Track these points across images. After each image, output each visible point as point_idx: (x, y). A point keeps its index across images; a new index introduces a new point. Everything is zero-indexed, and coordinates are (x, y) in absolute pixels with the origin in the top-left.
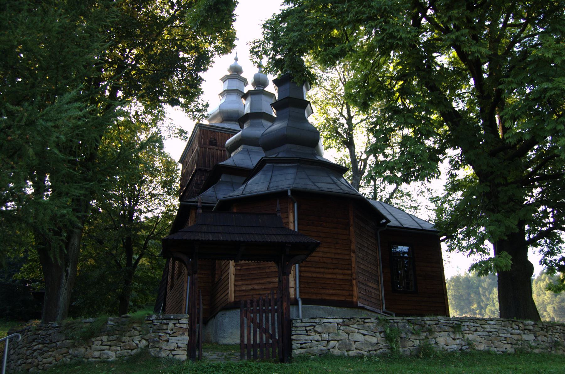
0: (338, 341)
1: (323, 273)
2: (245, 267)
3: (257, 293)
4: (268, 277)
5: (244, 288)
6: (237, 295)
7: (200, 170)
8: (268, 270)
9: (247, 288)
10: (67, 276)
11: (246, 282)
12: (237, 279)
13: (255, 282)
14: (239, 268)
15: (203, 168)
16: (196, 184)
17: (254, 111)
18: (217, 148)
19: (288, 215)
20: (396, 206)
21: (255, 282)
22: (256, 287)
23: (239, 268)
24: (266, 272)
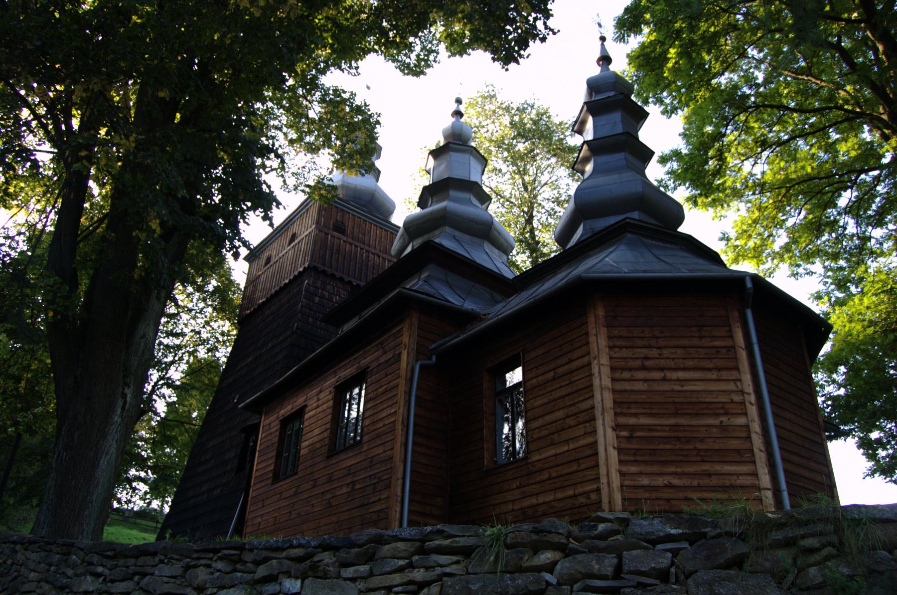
2: (639, 434)
3: (681, 495)
4: (703, 461)
5: (645, 481)
6: (627, 495)
8: (700, 446)
9: (654, 483)
10: (123, 408)
11: (649, 469)
12: (623, 458)
13: (672, 469)
14: (624, 433)
17: (600, 135)
18: (345, 239)
19: (730, 331)
20: (269, 426)
21: (672, 469)
22: (676, 482)
23: (624, 433)
24: (696, 449)
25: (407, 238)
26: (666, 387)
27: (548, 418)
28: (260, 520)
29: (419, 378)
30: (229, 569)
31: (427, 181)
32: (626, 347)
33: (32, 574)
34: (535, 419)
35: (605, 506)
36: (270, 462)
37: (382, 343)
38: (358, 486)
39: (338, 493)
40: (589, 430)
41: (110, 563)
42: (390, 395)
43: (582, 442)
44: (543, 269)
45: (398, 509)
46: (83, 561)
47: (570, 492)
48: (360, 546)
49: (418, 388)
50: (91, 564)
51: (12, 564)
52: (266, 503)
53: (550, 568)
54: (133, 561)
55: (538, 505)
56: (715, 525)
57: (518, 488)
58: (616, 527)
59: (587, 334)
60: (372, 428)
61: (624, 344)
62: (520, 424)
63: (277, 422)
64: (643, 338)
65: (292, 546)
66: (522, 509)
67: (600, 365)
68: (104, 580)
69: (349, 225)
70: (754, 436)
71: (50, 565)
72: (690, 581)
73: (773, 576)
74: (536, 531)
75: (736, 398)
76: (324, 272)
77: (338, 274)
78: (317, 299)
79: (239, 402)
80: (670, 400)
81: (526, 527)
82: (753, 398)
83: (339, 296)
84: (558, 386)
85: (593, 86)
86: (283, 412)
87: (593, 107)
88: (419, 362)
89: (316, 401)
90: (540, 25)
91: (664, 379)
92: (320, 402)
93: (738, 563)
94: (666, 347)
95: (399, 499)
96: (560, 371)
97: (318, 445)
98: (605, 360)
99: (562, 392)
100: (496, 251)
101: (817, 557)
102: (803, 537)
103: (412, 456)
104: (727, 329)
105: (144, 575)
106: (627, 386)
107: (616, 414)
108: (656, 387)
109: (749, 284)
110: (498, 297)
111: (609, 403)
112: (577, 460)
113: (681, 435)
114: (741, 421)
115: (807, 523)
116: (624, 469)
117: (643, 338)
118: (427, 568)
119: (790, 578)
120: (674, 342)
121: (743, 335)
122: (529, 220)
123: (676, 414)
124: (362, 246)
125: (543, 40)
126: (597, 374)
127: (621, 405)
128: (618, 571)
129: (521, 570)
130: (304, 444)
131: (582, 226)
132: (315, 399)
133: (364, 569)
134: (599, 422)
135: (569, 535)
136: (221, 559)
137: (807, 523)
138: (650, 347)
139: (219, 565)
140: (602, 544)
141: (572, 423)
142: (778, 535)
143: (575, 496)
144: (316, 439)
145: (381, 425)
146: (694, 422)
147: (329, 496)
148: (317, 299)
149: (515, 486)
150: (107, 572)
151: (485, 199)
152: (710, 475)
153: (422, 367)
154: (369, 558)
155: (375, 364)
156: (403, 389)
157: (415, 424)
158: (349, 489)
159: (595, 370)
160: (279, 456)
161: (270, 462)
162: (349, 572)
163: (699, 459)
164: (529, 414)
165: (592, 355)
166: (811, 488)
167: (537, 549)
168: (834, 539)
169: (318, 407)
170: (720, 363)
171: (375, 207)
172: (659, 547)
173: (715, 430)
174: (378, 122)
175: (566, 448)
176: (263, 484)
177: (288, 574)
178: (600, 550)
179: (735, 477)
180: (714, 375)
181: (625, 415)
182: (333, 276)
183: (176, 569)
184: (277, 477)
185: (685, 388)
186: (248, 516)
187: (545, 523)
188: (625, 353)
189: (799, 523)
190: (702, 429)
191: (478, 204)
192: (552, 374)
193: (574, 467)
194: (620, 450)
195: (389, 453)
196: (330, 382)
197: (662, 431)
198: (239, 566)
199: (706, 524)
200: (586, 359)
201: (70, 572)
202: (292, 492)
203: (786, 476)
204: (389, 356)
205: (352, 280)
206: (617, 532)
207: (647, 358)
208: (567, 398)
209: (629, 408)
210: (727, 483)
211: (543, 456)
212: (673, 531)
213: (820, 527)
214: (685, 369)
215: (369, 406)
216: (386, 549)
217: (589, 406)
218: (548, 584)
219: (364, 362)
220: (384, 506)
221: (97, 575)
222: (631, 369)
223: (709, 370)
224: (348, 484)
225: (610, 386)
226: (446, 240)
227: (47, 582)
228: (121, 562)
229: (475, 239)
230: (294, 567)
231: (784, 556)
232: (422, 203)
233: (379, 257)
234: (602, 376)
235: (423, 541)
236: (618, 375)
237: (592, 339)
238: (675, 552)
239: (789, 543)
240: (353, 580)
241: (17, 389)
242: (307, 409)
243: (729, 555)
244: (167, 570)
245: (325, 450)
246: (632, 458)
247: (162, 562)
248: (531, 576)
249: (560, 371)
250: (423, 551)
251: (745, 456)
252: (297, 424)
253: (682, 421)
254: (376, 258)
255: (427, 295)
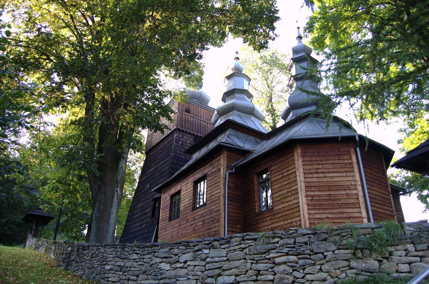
0: (339, 269)
1: (379, 208)
4: (340, 208)
5: (318, 216)
7: (179, 129)
8: (339, 202)
10: (117, 196)
12: (309, 208)
13: (328, 211)
14: (310, 198)
15: (181, 129)
16: (176, 139)
18: (190, 115)
19: (351, 156)
20: (165, 198)
22: (330, 216)
23: (310, 198)
24: (337, 203)
25: (218, 116)
26: (325, 180)
27: (281, 193)
28: (165, 237)
29: (228, 178)
30: (185, 248)
31: (225, 90)
32: (310, 165)
33: (110, 256)
34: (275, 193)
35: (303, 226)
36: (167, 213)
37: (212, 164)
38: (206, 222)
39: (198, 225)
40: (296, 197)
41: (142, 250)
42: (217, 185)
43: (293, 202)
44: (276, 131)
45: (223, 230)
46: (131, 250)
47: (290, 221)
48: (225, 239)
49: (228, 182)
50: (135, 250)
51: (98, 253)
52: (167, 230)
53: (277, 243)
54: (151, 248)
55: (278, 226)
56: (320, 230)
57: (270, 220)
58: (294, 231)
59: (294, 160)
60: (210, 198)
61: (308, 163)
62: (270, 192)
63: (169, 196)
64: (316, 161)
65: (205, 241)
66: (271, 228)
67: (299, 172)
68: (141, 255)
69: (192, 109)
70: (360, 198)
71: (117, 252)
72: (312, 244)
73: (334, 243)
74: (273, 233)
75: (353, 183)
76: (182, 131)
77: (188, 131)
78: (180, 143)
79: (150, 188)
80: (327, 185)
81: (271, 232)
82: (359, 183)
83: (189, 141)
84: (283, 180)
85: (295, 51)
86: (171, 192)
87: (296, 60)
88: (228, 172)
89: (185, 187)
90: (271, 33)
91: (325, 177)
92: (187, 188)
93: (325, 240)
94: (325, 164)
95: (223, 226)
96: (284, 174)
97: (188, 206)
98: (301, 170)
99: (286, 183)
100: (257, 119)
101: (346, 238)
102: (342, 233)
103: (228, 209)
104: (349, 156)
105: (155, 252)
106: (310, 180)
107: (306, 191)
108: (321, 180)
109: (357, 138)
110: (258, 140)
111: (303, 187)
112: (292, 209)
113: (331, 198)
114: (355, 192)
115: (344, 229)
116: (310, 212)
117: (316, 161)
118: (245, 244)
119: (338, 244)
120: (329, 162)
121: (355, 158)
122: (270, 101)
123: (329, 190)
124: (198, 118)
125: (274, 39)
126: (298, 176)
127: (308, 187)
128: (295, 243)
129: (270, 243)
130: (181, 206)
131: (292, 113)
132: (185, 187)
133: (227, 245)
134: (300, 194)
135: (282, 234)
136: (182, 246)
137: (344, 229)
138: (319, 164)
139: (182, 247)
140: (291, 236)
141: (290, 195)
142: (336, 232)
143: (291, 223)
144: (187, 203)
145: (214, 197)
146: (336, 193)
147: (194, 226)
148: (180, 143)
149: (268, 219)
150: (141, 252)
151: (250, 96)
152: (343, 213)
153: (229, 173)
154: (229, 242)
155: (210, 172)
156: (222, 182)
157: (228, 197)
158: (202, 223)
159: (298, 174)
160: (171, 210)
161: (167, 213)
162: (223, 247)
163: (338, 207)
164: (273, 188)
165: (296, 168)
166: (385, 216)
167: (274, 238)
168: (350, 233)
169: (187, 190)
170: (346, 169)
171: (202, 100)
172: (305, 236)
173: (344, 196)
174: (204, 66)
175: (287, 204)
176: (165, 222)
177: (205, 248)
178: (290, 238)
179: (353, 214)
180: (344, 174)
181: (310, 191)
182: (186, 132)
183: (167, 249)
184: (170, 219)
185: (333, 180)
186: (159, 235)
187: (276, 231)
188: (309, 167)
189: (341, 229)
190: (340, 195)
191: (248, 100)
192: (281, 176)
193: (291, 212)
194: (308, 205)
195: (218, 208)
196: (190, 180)
197: (324, 197)
198: (188, 247)
199: (318, 230)
200: (294, 170)
201: (126, 253)
202: (178, 225)
203: (372, 212)
204: (216, 169)
205: (194, 133)
206: (295, 233)
207: (318, 169)
208: (287, 185)
209: (311, 188)
210: (349, 216)
211: (279, 208)
212: (309, 232)
213: (346, 230)
214: (332, 172)
215: (209, 189)
216: (233, 240)
217: (296, 188)
218: (277, 246)
219: (205, 172)
220: (217, 229)
221: (138, 254)
222: (311, 173)
223: (342, 172)
224: (202, 221)
225: (303, 180)
226: (234, 117)
227: (117, 257)
228: (146, 249)
229: (247, 115)
230: (206, 246)
231: (337, 238)
232: (224, 100)
233: (205, 122)
234: (300, 177)
235: (243, 237)
236: (306, 176)
237: (296, 162)
238: (309, 238)
239: (338, 234)
240: (224, 248)
241: (69, 189)
242: (182, 191)
243: (323, 238)
244: (163, 250)
245: (191, 207)
246: (313, 208)
247: (161, 248)
248: (272, 245)
249: (284, 174)
250: (243, 240)
251: (356, 205)
252: (178, 197)
253: (332, 193)
254: (204, 123)
255: (230, 144)
